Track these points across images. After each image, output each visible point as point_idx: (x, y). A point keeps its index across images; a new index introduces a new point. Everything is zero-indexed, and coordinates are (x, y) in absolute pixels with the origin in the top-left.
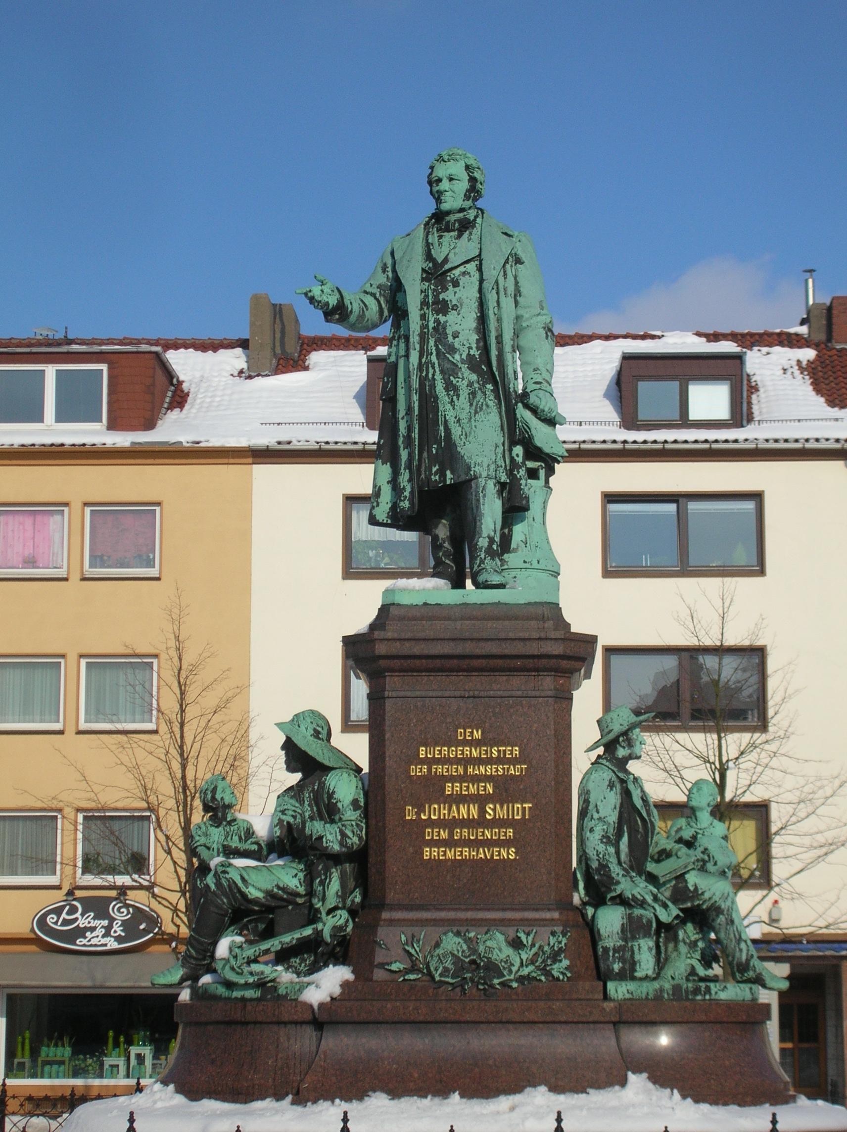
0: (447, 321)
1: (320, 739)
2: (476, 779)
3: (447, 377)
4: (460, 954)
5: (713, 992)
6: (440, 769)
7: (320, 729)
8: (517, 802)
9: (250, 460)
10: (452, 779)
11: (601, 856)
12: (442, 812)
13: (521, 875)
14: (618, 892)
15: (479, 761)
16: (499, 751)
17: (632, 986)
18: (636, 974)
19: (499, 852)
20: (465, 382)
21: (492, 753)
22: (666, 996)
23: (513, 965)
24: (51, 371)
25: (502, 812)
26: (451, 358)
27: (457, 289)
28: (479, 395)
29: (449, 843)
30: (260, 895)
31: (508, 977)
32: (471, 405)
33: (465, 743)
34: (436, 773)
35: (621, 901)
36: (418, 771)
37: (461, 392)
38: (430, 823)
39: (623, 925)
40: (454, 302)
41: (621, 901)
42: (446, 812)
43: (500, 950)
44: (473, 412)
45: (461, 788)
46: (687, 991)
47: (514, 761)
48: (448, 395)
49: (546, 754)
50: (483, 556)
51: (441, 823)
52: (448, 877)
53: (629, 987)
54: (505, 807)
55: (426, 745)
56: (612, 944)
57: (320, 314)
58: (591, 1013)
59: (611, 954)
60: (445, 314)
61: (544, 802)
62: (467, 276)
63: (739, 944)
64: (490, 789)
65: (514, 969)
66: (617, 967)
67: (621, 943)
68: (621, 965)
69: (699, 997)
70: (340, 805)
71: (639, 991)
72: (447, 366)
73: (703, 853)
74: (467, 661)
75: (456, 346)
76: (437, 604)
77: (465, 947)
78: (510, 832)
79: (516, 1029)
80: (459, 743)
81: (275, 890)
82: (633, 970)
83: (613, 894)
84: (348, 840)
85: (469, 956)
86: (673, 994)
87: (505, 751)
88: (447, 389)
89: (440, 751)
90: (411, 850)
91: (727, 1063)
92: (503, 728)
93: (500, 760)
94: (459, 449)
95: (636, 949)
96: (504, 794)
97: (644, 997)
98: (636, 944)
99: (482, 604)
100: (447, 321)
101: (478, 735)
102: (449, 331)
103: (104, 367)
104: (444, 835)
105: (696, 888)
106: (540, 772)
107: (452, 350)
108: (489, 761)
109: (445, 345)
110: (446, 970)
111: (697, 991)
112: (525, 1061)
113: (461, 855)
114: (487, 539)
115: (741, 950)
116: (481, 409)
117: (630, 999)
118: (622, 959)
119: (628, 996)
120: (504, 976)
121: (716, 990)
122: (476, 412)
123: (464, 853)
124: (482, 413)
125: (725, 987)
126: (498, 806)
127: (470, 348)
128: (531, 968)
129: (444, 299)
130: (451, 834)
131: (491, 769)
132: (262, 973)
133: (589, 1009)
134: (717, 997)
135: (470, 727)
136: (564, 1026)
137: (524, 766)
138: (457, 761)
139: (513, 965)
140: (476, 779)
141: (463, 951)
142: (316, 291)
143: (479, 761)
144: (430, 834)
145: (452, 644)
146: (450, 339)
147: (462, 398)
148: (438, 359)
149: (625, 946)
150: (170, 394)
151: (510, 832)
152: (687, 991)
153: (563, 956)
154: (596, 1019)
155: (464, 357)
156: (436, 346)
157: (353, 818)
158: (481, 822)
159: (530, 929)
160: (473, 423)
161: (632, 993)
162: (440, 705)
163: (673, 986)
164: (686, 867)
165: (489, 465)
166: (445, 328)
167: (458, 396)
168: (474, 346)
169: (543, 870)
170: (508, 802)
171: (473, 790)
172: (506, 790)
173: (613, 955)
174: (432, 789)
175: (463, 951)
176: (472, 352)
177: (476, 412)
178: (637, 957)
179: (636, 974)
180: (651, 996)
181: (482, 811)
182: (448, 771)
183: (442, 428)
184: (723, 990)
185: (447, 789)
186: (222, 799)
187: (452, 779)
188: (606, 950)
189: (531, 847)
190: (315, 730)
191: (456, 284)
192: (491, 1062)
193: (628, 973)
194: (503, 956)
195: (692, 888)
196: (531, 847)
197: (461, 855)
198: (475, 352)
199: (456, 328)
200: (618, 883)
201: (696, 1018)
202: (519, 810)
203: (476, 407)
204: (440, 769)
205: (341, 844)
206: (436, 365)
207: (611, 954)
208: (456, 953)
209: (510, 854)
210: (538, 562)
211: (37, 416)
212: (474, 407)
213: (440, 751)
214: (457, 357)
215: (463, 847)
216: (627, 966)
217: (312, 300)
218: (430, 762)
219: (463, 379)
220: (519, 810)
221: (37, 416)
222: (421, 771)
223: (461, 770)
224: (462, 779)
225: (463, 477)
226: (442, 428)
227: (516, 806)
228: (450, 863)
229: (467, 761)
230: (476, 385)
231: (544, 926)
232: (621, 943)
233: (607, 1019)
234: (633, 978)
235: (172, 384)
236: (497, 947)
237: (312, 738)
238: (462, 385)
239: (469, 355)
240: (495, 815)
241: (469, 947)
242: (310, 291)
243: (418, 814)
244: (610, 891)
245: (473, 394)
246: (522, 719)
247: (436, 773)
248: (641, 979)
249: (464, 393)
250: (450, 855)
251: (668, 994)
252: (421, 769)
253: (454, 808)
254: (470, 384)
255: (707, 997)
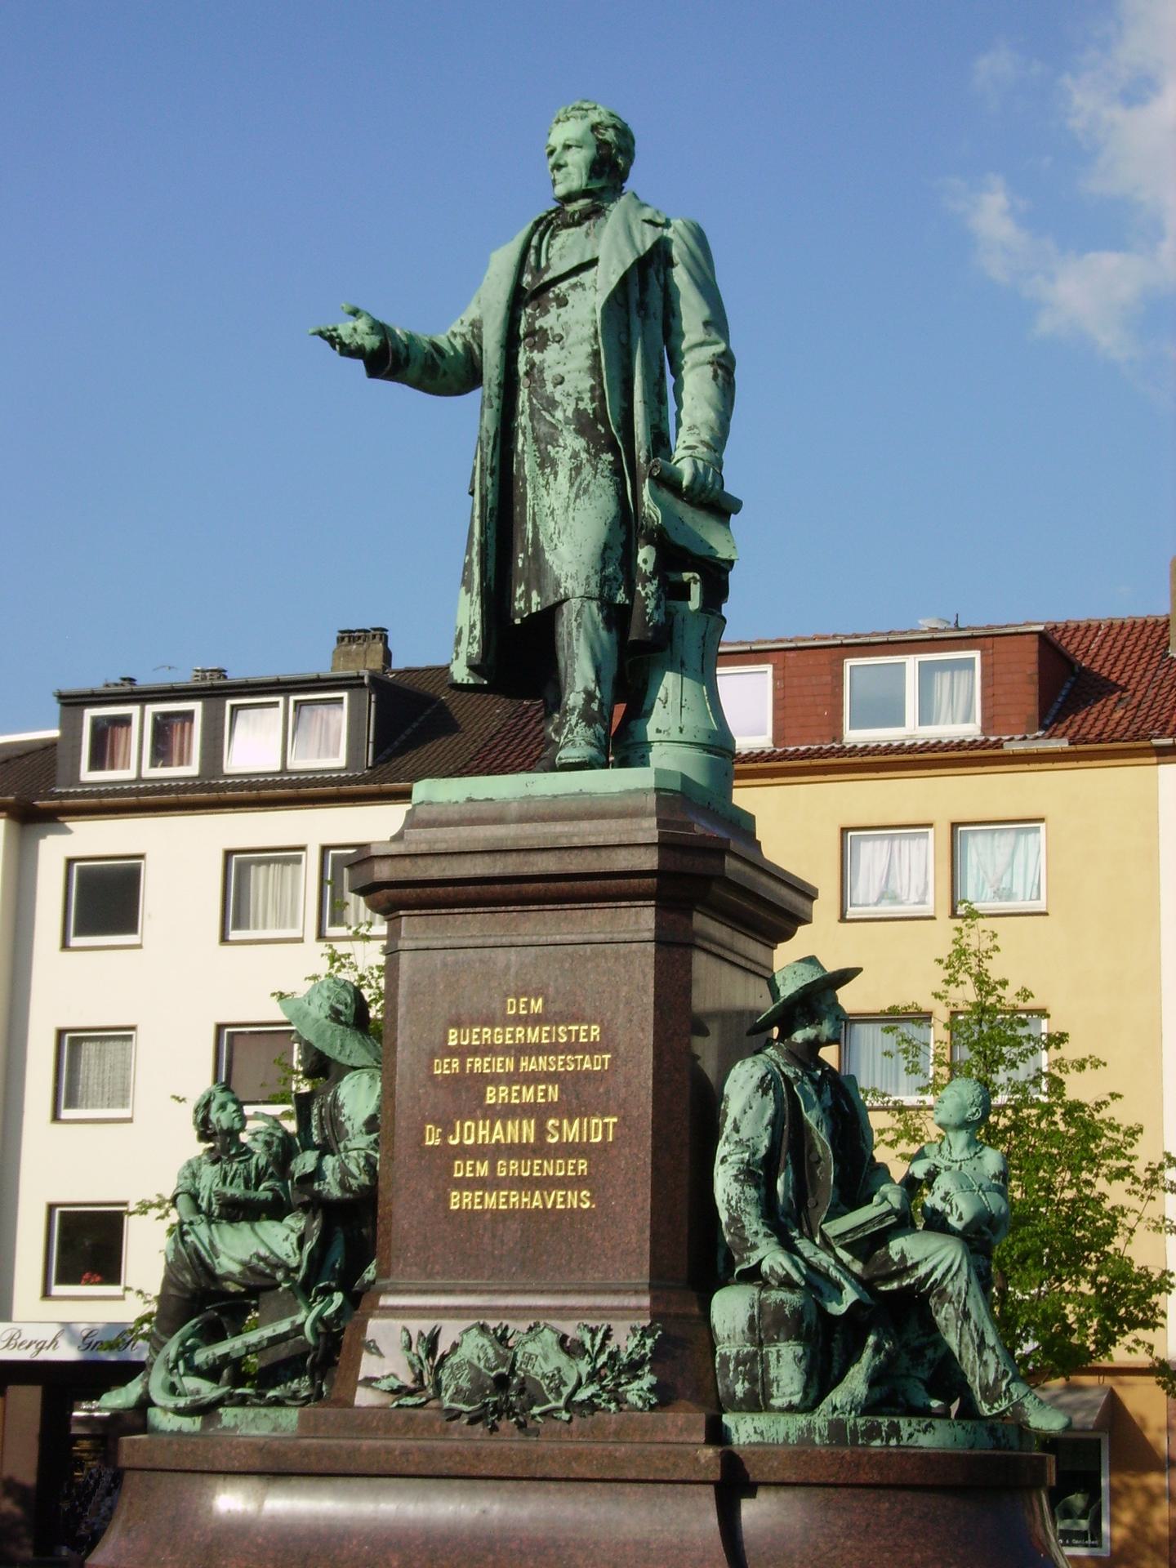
0: (543, 361)
1: (341, 1023)
2: (532, 1079)
3: (543, 446)
4: (482, 1365)
5: (905, 1434)
6: (479, 1064)
7: (341, 1007)
8: (594, 1115)
9: (1154, 760)
10: (495, 1079)
11: (733, 1203)
12: (481, 1133)
13: (597, 1235)
14: (753, 1263)
15: (538, 1050)
16: (569, 1033)
17: (761, 1421)
18: (773, 1402)
19: (565, 1197)
20: (568, 453)
21: (557, 1034)
22: (817, 1439)
23: (565, 1384)
24: (911, 663)
25: (572, 1132)
26: (548, 417)
27: (562, 310)
28: (587, 470)
29: (490, 1184)
30: (236, 1268)
31: (553, 1404)
32: (572, 485)
33: (518, 1020)
34: (472, 1069)
35: (753, 1275)
36: (445, 1067)
37: (560, 468)
38: (463, 1152)
39: (752, 1318)
40: (558, 330)
41: (753, 1275)
42: (487, 1132)
43: (546, 1358)
44: (572, 496)
45: (510, 1094)
46: (854, 1432)
47: (591, 1048)
48: (543, 474)
49: (641, 1035)
50: (573, 722)
51: (478, 1152)
52: (486, 1240)
53: (756, 1423)
54: (577, 1122)
55: (458, 1024)
56: (734, 1351)
57: (359, 365)
58: (676, 1465)
59: (731, 1367)
60: (541, 351)
61: (636, 1114)
62: (579, 290)
63: (980, 1354)
64: (554, 1093)
65: (566, 1391)
66: (740, 1389)
67: (749, 1348)
68: (747, 1385)
69: (877, 1443)
70: (348, 1125)
71: (773, 1430)
72: (543, 429)
73: (944, 1199)
74: (515, 887)
75: (558, 397)
76: (487, 800)
77: (491, 1352)
78: (583, 1165)
79: (560, 1490)
80: (507, 1021)
81: (255, 1261)
82: (768, 1396)
83: (745, 1266)
84: (353, 1182)
85: (496, 1367)
86: (829, 1437)
87: (577, 1032)
88: (542, 466)
89: (479, 1034)
90: (431, 1194)
91: (918, 1556)
92: (575, 994)
93: (572, 1048)
94: (547, 556)
95: (773, 1358)
96: (574, 1101)
97: (781, 1441)
98: (773, 1350)
99: (555, 797)
100: (543, 361)
101: (537, 1006)
102: (548, 375)
103: (976, 655)
104: (483, 1170)
105: (903, 1257)
106: (630, 1065)
107: (552, 404)
108: (553, 1049)
109: (540, 397)
110: (458, 1390)
111: (873, 1432)
112: (567, 1545)
113: (507, 1202)
114: (583, 695)
115: (985, 1364)
116: (586, 491)
117: (758, 1444)
118: (752, 1378)
119: (755, 1438)
120: (548, 1402)
121: (910, 1430)
122: (577, 496)
123: (512, 1200)
124: (585, 498)
125: (930, 1425)
126: (565, 1122)
127: (579, 399)
128: (593, 1389)
129: (541, 328)
130: (493, 1168)
131: (556, 1063)
132: (198, 1392)
133: (672, 1459)
134: (911, 1442)
135: (525, 994)
136: (635, 1487)
137: (607, 1057)
138: (505, 1050)
139: (565, 1384)
140: (532, 1079)
141: (488, 1360)
142: (344, 330)
143: (538, 1050)
144: (462, 1169)
145: (487, 859)
146: (549, 387)
147: (561, 476)
148: (531, 420)
149: (755, 1354)
150: (1068, 685)
151: (583, 1165)
152: (854, 1432)
153: (647, 1368)
154: (683, 1477)
155: (569, 413)
156: (530, 400)
157: (362, 1145)
158: (540, 1149)
159: (599, 1324)
160: (571, 513)
161: (762, 1433)
162: (481, 961)
163: (831, 1422)
164: (881, 1221)
165: (588, 577)
166: (541, 371)
167: (556, 474)
168: (587, 396)
169: (632, 1226)
170: (582, 1115)
171: (528, 1095)
172: (578, 1095)
173: (736, 1369)
174: (465, 1097)
175: (488, 1360)
176: (582, 406)
177: (577, 496)
178: (773, 1373)
179: (773, 1402)
180: (792, 1439)
181: (541, 1132)
182: (490, 1067)
183: (529, 526)
184: (925, 1431)
185: (489, 1095)
186: (218, 1120)
187: (495, 1079)
188: (725, 1360)
189: (614, 1187)
190: (332, 1007)
191: (562, 302)
192: (513, 1546)
193: (757, 1402)
194: (549, 1369)
195: (896, 1259)
196: (614, 1187)
197: (507, 1202)
198: (587, 405)
199: (560, 370)
200: (754, 1247)
201: (864, 1478)
202: (598, 1129)
203: (579, 489)
204: (479, 1064)
205: (342, 1185)
206: (529, 430)
207: (731, 1367)
208: (476, 1362)
209: (580, 1200)
210: (681, 730)
211: (900, 721)
212: (574, 489)
213: (479, 1034)
214: (559, 414)
215: (510, 1189)
216: (759, 1389)
217: (332, 340)
218: (462, 1052)
219: (565, 448)
220: (598, 1129)
221: (900, 721)
222: (449, 1068)
223: (510, 1065)
224: (512, 1078)
225: (553, 600)
226: (529, 526)
227: (594, 1121)
228: (488, 1216)
229: (523, 1050)
230: (584, 455)
231: (623, 1318)
232: (749, 1348)
233: (701, 1477)
234: (769, 1408)
235: (1073, 674)
236: (541, 1358)
237: (327, 1022)
238: (563, 457)
239: (577, 410)
240: (561, 1137)
241: (497, 1353)
242: (335, 330)
243: (443, 1136)
244: (742, 1260)
245: (578, 469)
246: (605, 980)
247: (472, 1069)
248: (782, 1410)
249: (563, 472)
250: (490, 1202)
251: (821, 1436)
252: (450, 1064)
253: (498, 1125)
254: (575, 455)
255: (893, 1442)
